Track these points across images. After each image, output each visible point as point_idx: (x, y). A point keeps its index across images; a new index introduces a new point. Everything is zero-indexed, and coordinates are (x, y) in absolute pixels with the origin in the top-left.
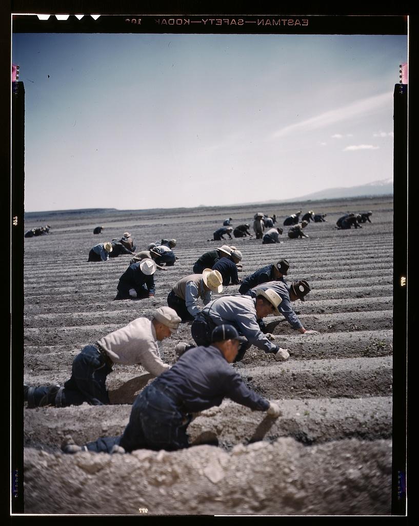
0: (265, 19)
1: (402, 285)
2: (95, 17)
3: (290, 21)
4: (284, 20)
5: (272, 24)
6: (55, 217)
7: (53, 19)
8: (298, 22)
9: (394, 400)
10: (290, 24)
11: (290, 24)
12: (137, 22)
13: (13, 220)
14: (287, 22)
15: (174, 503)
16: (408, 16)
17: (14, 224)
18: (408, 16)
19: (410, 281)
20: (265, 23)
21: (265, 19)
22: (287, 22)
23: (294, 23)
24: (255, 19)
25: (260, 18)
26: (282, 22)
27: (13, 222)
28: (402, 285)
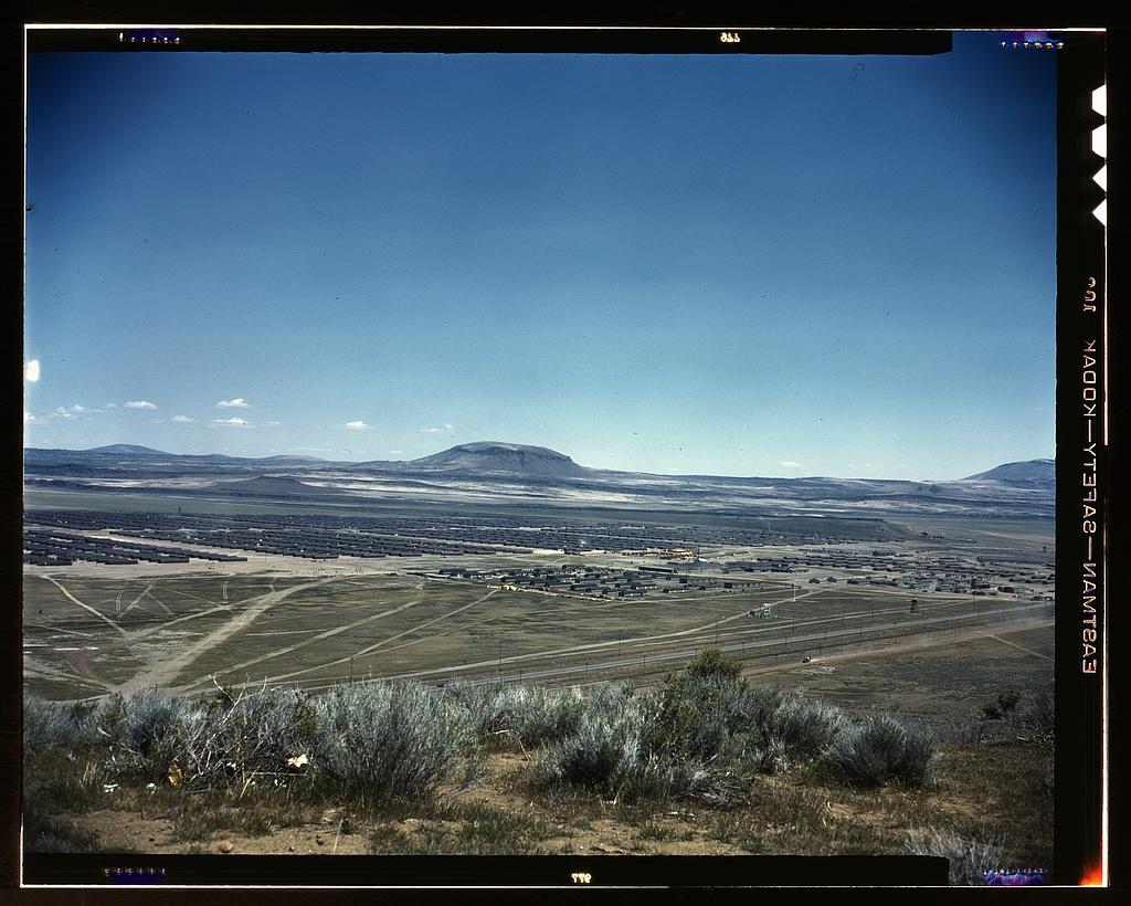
0: (1098, 580)
1: (574, 876)
2: (1101, 213)
3: (1092, 634)
4: (1094, 622)
5: (1085, 595)
6: (858, 494)
7: (1097, 120)
8: (1090, 650)
9: (18, 665)
10: (1087, 634)
11: (1087, 634)
12: (1091, 304)
13: (733, 32)
14: (1090, 626)
15: (564, 698)
16: (1104, 30)
17: (724, 35)
18: (1104, 30)
19: (583, 894)
20: (1087, 579)
21: (1098, 580)
22: (1090, 626)
23: (1089, 643)
24: (1097, 558)
25: (1098, 570)
26: (1090, 616)
27: (727, 32)
28: (574, 876)
